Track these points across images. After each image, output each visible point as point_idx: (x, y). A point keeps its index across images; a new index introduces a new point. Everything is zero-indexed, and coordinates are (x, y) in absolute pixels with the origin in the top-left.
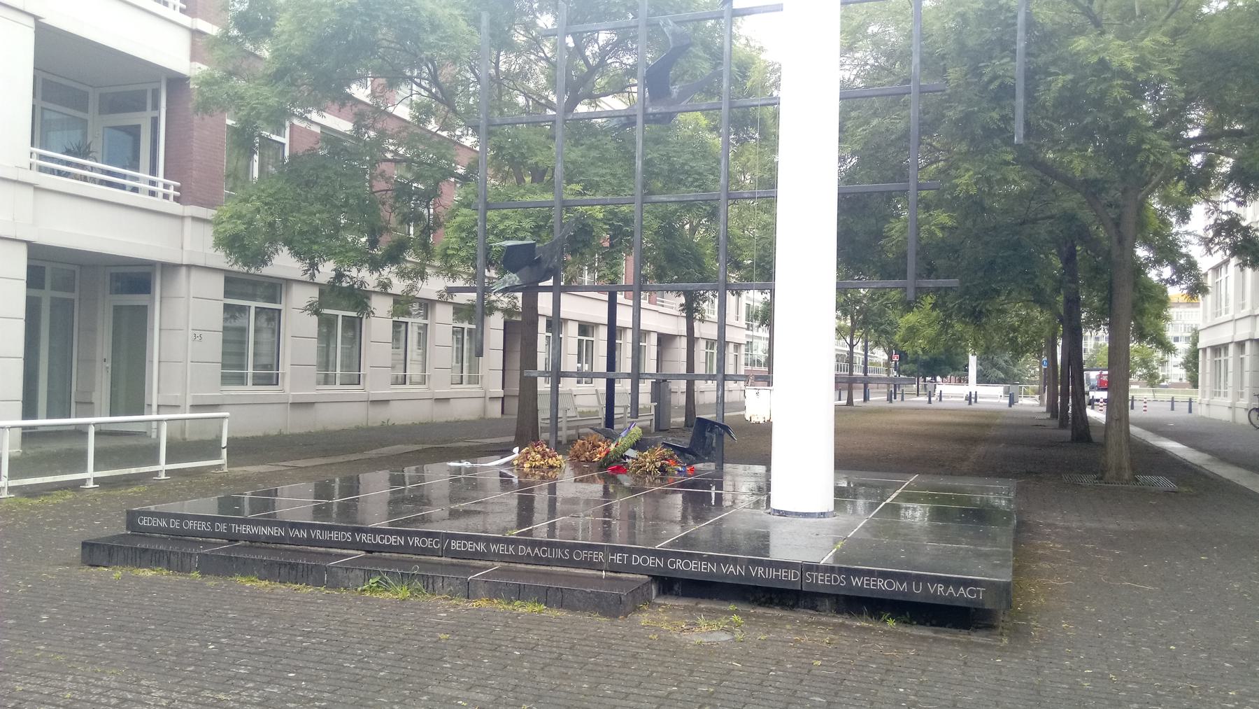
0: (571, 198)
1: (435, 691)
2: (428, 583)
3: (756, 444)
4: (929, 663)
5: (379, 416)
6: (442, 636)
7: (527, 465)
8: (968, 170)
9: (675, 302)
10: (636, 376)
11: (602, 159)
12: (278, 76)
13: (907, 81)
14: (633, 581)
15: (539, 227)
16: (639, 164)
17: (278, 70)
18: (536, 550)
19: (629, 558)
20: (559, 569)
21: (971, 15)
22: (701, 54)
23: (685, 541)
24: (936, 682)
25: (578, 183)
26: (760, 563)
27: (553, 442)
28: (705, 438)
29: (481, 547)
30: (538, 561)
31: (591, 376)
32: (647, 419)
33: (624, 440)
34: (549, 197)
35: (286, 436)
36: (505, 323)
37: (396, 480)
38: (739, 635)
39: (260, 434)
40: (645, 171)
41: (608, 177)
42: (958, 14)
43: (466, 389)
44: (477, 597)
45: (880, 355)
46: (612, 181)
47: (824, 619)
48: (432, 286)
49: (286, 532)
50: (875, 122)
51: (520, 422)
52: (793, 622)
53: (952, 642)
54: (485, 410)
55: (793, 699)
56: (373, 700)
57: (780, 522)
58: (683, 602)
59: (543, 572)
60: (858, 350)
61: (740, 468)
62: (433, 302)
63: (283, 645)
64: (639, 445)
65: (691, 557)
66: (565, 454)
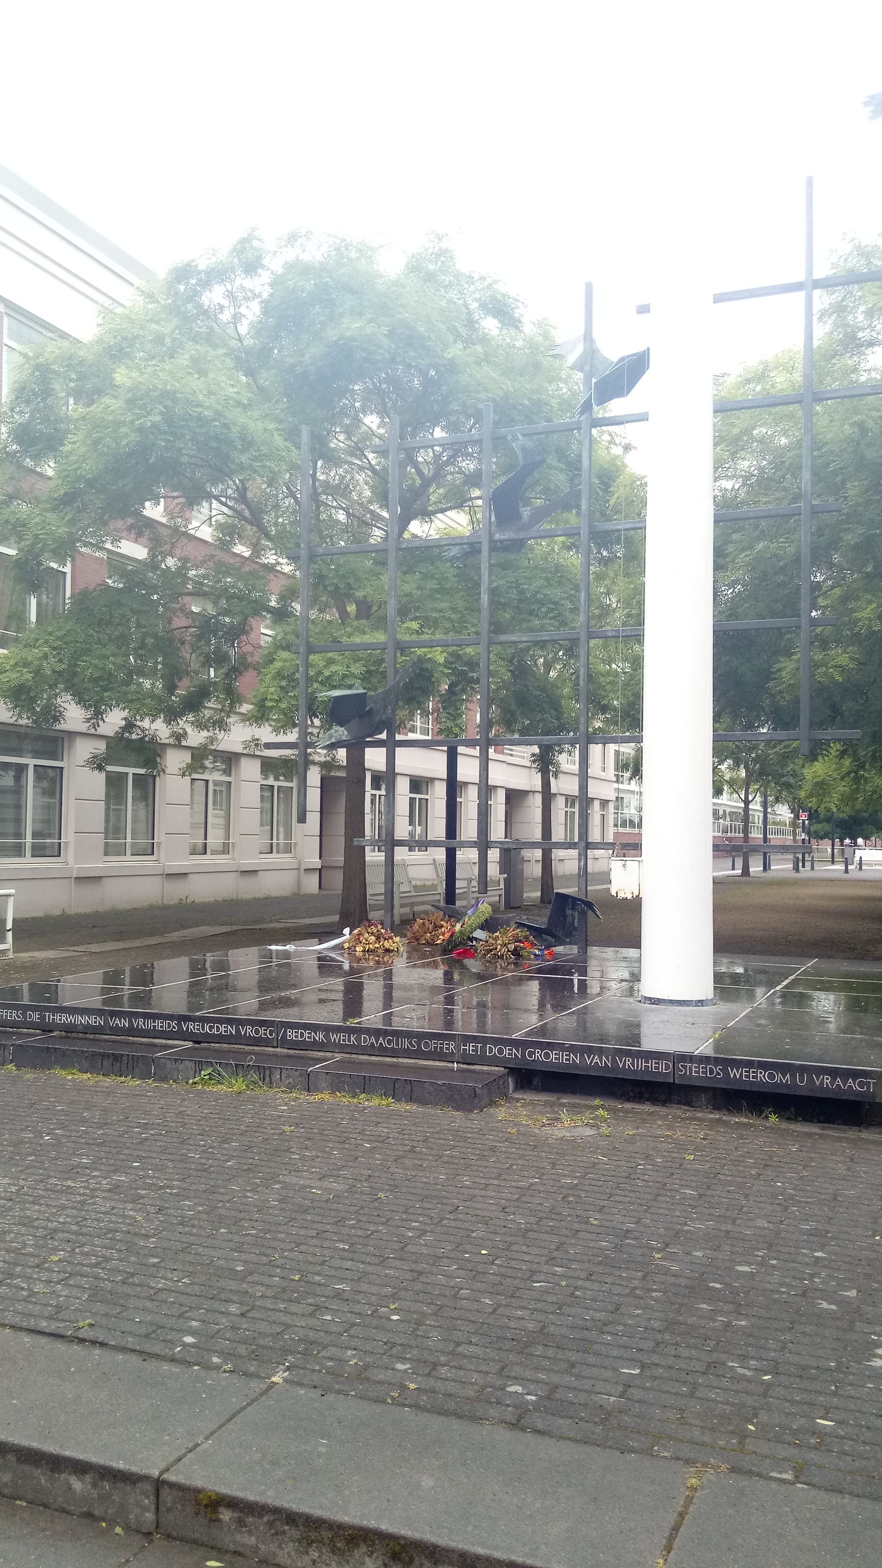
0: (407, 638)
1: (287, 1180)
2: (265, 1073)
3: (624, 923)
4: (812, 1159)
5: (176, 892)
6: (287, 1128)
7: (359, 949)
8: (870, 602)
9: (525, 753)
10: (483, 844)
11: (443, 591)
12: (67, 500)
13: (797, 497)
14: (488, 1073)
15: (369, 672)
16: (485, 598)
17: (66, 494)
18: (381, 1040)
19: (483, 1049)
20: (405, 1060)
21: (870, 424)
22: (555, 463)
23: (542, 1030)
24: (817, 1177)
25: (415, 619)
26: (628, 1054)
27: (388, 922)
28: (565, 916)
29: (320, 1036)
30: (382, 1051)
31: (424, 844)
32: (496, 894)
33: (471, 919)
34: (380, 637)
35: (70, 916)
36: (322, 779)
37: (197, 969)
38: (605, 1130)
39: (40, 914)
40: (491, 602)
41: (449, 613)
42: (854, 424)
43: (275, 859)
44: (318, 1090)
45: (783, 812)
46: (453, 616)
47: (699, 1115)
48: (236, 736)
49: (106, 1021)
50: (760, 546)
51: (345, 899)
52: (664, 1118)
53: (840, 1139)
54: (299, 884)
55: (662, 1191)
56: (224, 1188)
57: (652, 1010)
58: (543, 1097)
59: (392, 1065)
60: (756, 806)
61: (610, 952)
62: (237, 756)
63: (122, 1136)
64: (489, 925)
65: (551, 1046)
66: (403, 935)
